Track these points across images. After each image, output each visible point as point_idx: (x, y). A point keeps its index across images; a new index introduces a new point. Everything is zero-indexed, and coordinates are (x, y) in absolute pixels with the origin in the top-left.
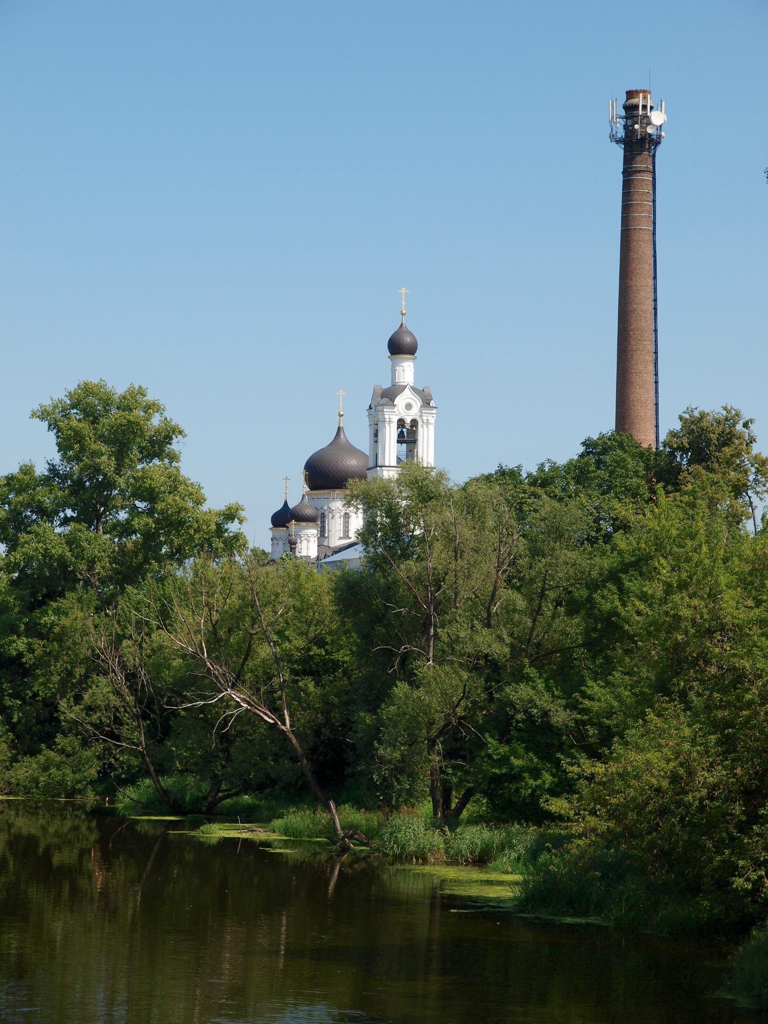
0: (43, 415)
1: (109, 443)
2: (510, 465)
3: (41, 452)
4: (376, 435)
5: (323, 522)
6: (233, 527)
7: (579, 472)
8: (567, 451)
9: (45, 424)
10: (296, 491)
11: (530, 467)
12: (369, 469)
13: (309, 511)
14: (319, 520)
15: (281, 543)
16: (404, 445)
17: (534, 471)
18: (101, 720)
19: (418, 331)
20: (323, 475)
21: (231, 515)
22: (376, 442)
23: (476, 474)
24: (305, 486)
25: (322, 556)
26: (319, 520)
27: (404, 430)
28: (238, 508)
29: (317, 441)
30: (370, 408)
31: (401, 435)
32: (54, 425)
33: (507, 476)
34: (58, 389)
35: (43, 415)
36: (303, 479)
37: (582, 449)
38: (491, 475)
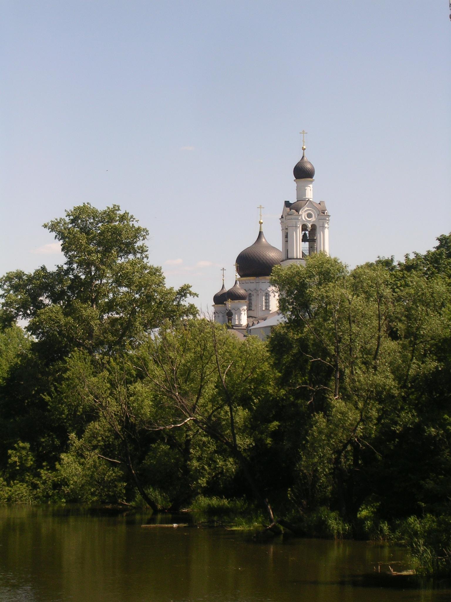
0: (53, 227)
1: (99, 239)
2: (387, 256)
3: (51, 256)
4: (287, 237)
5: (250, 300)
6: (186, 302)
7: (433, 259)
8: (427, 245)
9: (54, 234)
10: (230, 279)
11: (399, 259)
12: (282, 261)
13: (242, 292)
14: (247, 298)
15: (221, 315)
16: (307, 243)
17: (403, 261)
18: (91, 234)
19: (313, 161)
20: (251, 265)
21: (184, 291)
22: (287, 241)
23: (363, 263)
24: (237, 274)
25: (251, 324)
26: (247, 298)
27: (307, 232)
28: (188, 287)
29: (246, 242)
30: (282, 217)
31: (304, 236)
32: (61, 236)
33: (387, 263)
34: (60, 212)
35: (53, 227)
36: (235, 269)
37: (438, 243)
38: (372, 264)
